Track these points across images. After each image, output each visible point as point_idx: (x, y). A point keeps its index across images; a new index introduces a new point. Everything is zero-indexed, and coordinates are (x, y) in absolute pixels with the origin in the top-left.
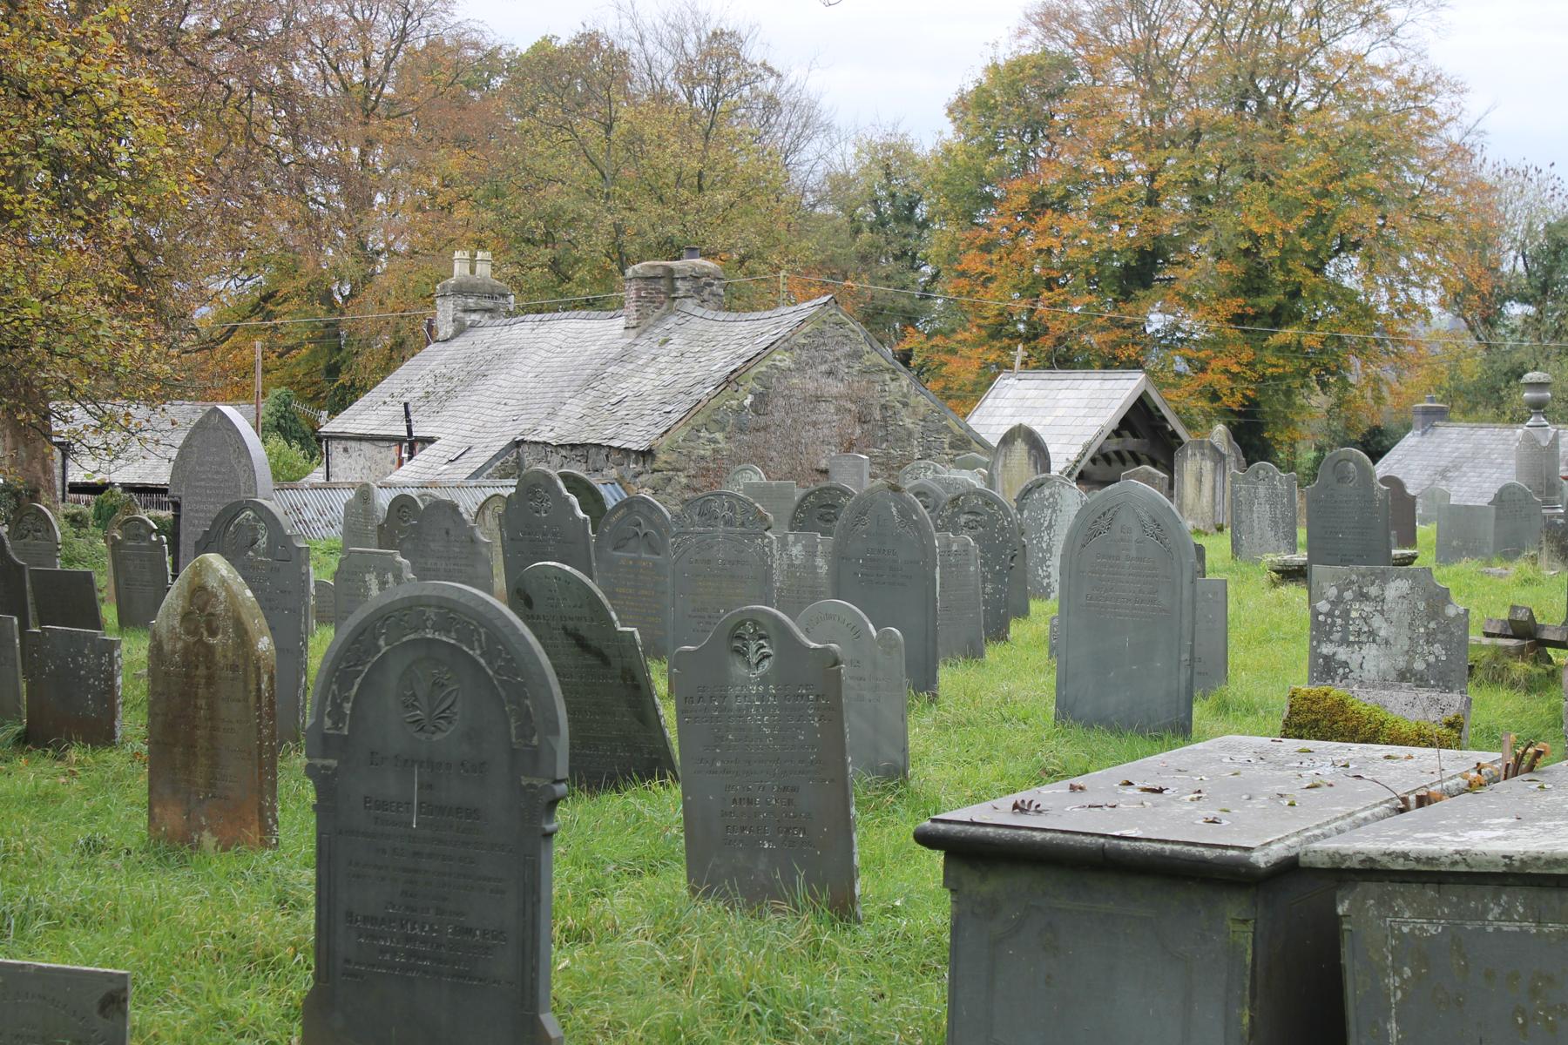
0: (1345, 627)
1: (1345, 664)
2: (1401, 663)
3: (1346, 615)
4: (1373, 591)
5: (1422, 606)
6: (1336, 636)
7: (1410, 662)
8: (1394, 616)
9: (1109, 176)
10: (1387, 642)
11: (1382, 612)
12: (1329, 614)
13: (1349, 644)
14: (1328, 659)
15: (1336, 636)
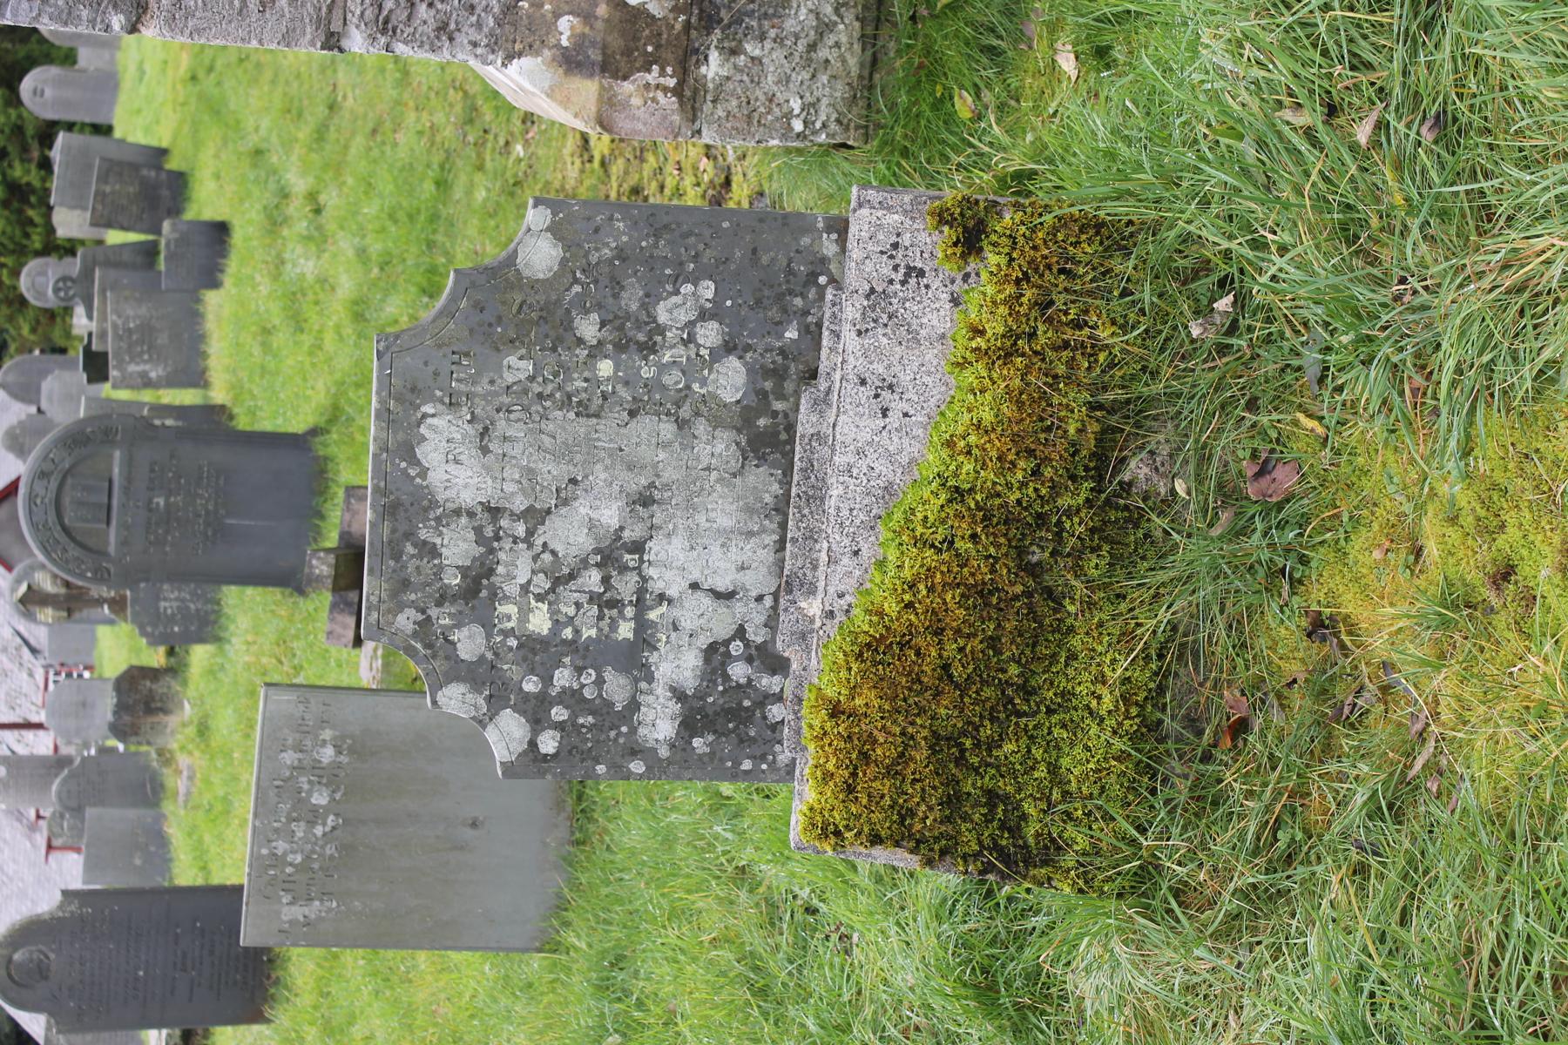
0: (585, 655)
1: (716, 655)
2: (718, 447)
3: (539, 653)
4: (457, 548)
5: (517, 367)
6: (617, 687)
7: (718, 416)
8: (552, 472)
9: (1252, 405)
10: (645, 500)
11: (536, 517)
12: (536, 712)
13: (645, 639)
14: (690, 724)
15: (617, 687)
